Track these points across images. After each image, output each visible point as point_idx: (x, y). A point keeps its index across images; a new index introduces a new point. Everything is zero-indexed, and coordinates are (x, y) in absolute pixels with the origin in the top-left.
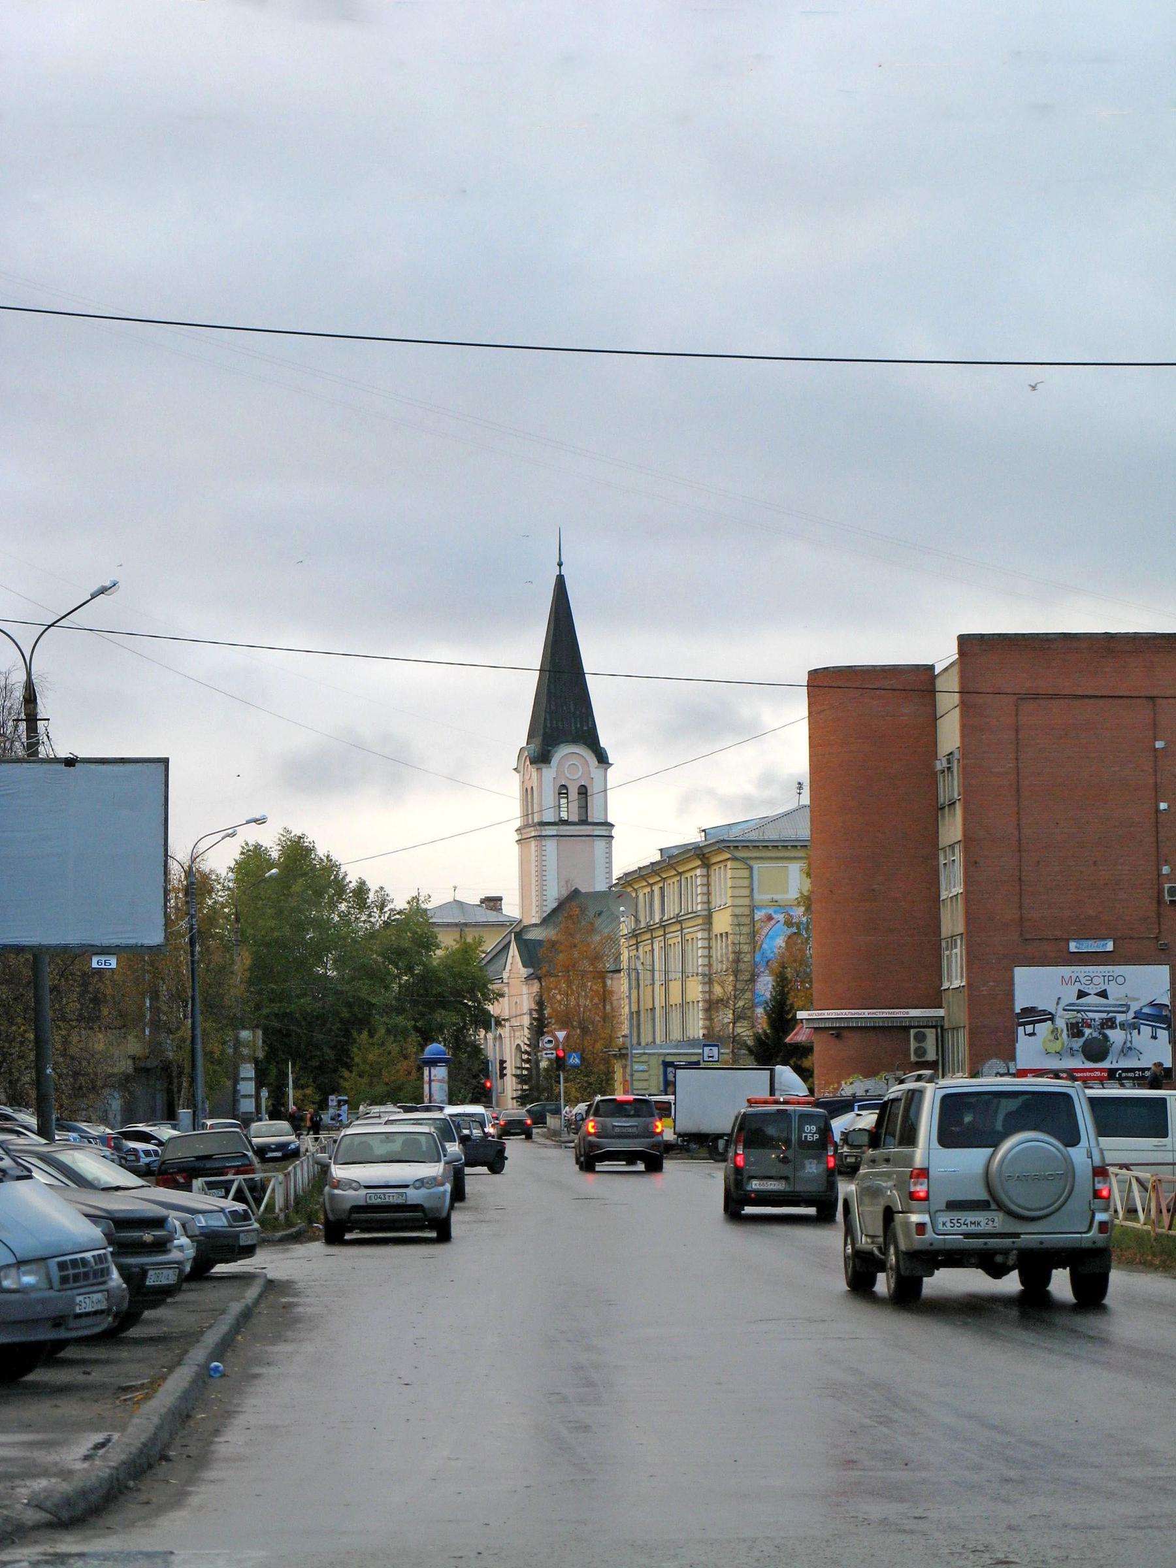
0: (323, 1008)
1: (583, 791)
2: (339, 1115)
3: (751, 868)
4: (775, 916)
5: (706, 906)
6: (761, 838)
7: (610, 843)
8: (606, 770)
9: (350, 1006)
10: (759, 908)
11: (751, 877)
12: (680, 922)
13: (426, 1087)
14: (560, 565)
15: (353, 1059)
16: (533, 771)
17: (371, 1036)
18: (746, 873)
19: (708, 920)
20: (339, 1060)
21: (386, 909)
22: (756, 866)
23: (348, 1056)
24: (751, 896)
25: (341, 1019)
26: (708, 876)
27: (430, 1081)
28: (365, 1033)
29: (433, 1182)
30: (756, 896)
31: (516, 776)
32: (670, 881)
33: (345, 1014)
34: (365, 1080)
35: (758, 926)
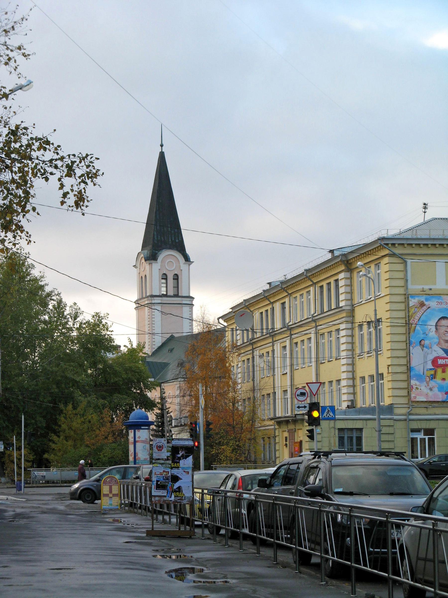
0: (37, 385)
1: (176, 278)
2: (175, 479)
3: (405, 262)
4: (426, 303)
5: (349, 303)
6: (415, 237)
7: (192, 308)
8: (189, 265)
9: (58, 384)
10: (413, 296)
11: (406, 270)
12: (315, 321)
13: (131, 447)
14: (162, 146)
15: (60, 426)
16: (146, 265)
17: (74, 408)
18: (400, 267)
19: (352, 313)
20: (48, 428)
21: (78, 319)
22: (409, 261)
23: (56, 424)
24: (406, 286)
25: (51, 393)
26: (351, 278)
27: (135, 442)
28: (70, 407)
29: (150, 528)
30: (410, 286)
31: (135, 270)
32: (294, 296)
33: (55, 390)
34: (70, 443)
35: (412, 311)
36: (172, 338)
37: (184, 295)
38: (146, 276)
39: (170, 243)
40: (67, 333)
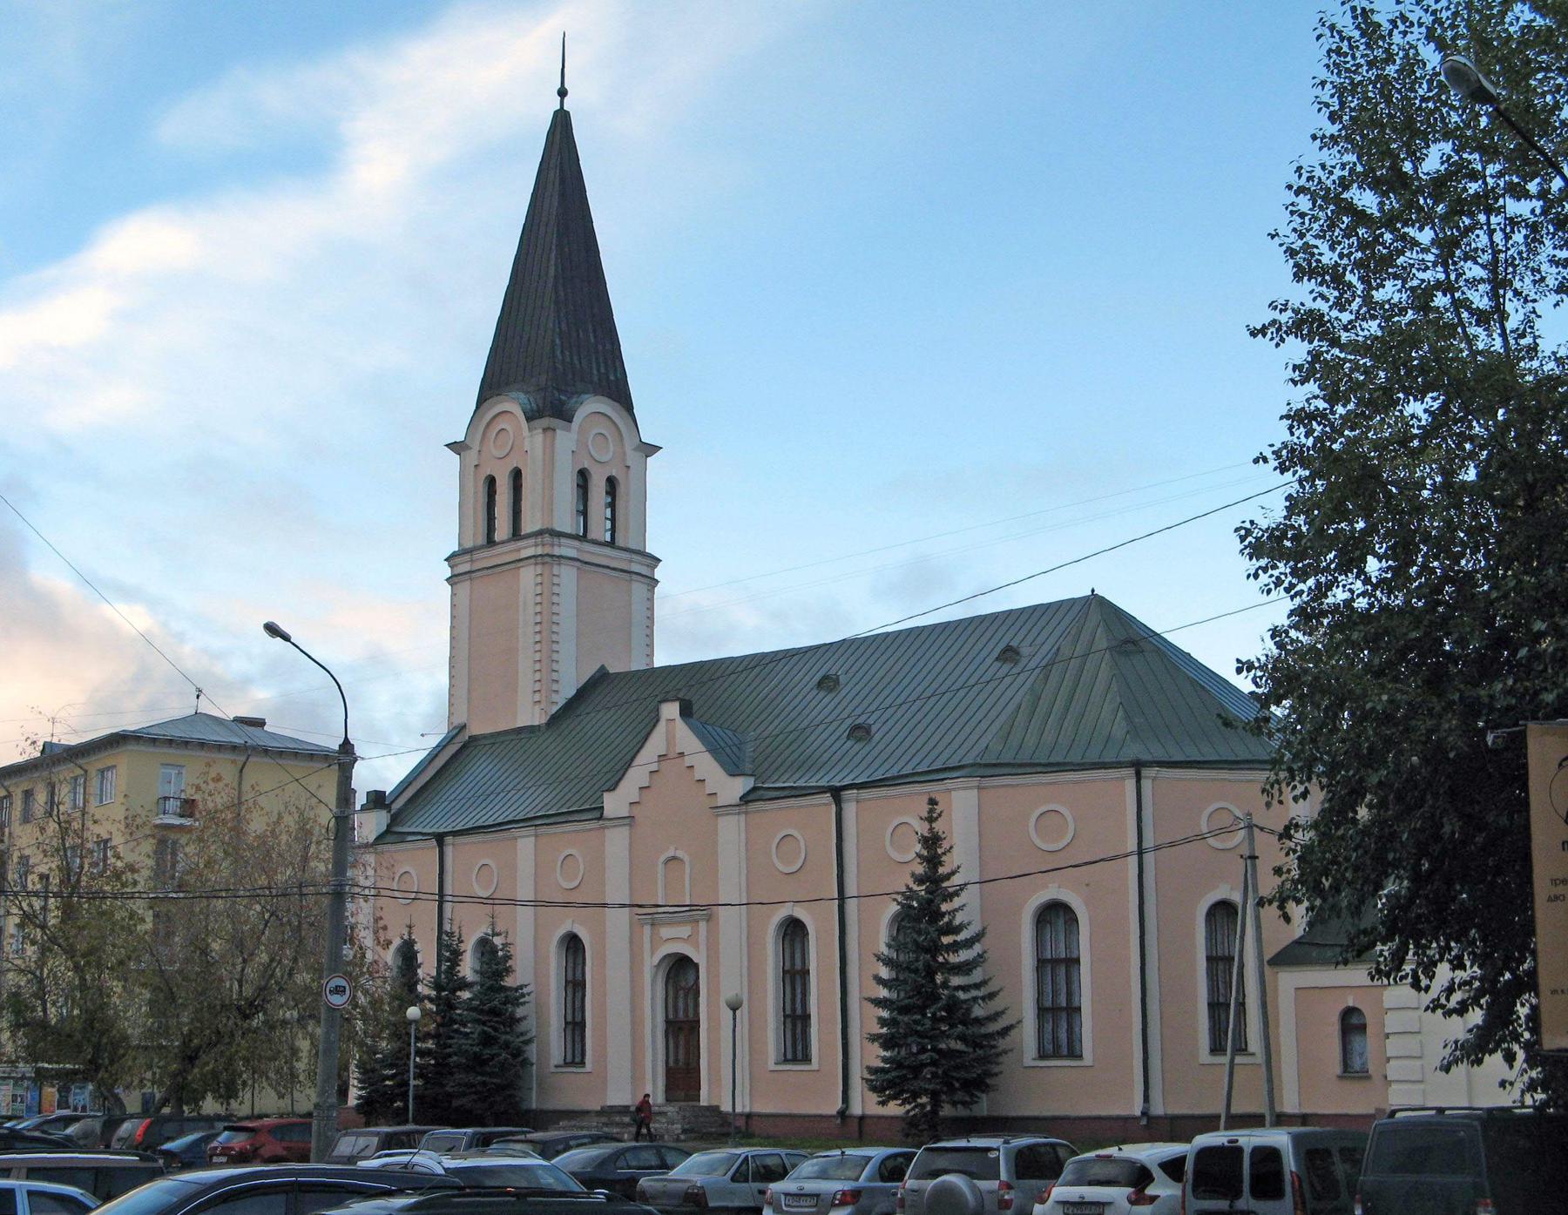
14: (562, 93)
36: (600, 680)
37: (632, 546)
38: (517, 475)
39: (596, 379)
40: (1485, 183)
